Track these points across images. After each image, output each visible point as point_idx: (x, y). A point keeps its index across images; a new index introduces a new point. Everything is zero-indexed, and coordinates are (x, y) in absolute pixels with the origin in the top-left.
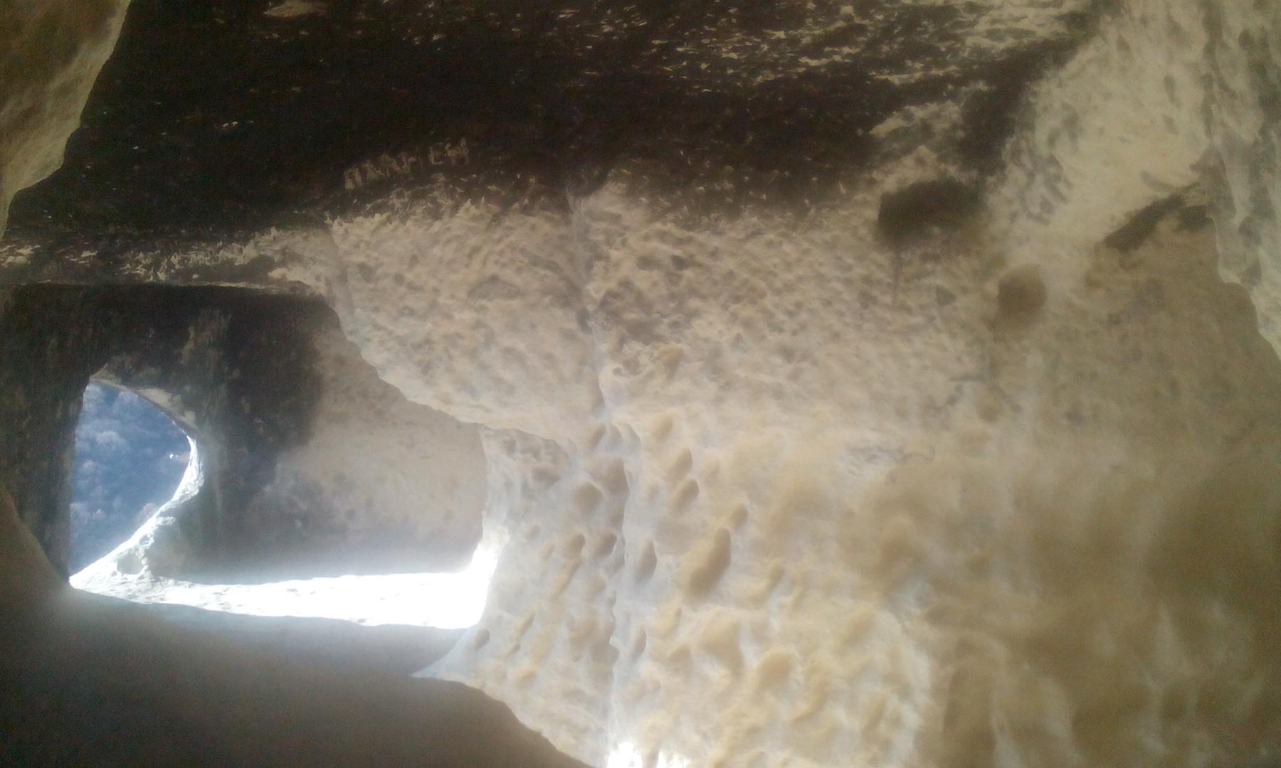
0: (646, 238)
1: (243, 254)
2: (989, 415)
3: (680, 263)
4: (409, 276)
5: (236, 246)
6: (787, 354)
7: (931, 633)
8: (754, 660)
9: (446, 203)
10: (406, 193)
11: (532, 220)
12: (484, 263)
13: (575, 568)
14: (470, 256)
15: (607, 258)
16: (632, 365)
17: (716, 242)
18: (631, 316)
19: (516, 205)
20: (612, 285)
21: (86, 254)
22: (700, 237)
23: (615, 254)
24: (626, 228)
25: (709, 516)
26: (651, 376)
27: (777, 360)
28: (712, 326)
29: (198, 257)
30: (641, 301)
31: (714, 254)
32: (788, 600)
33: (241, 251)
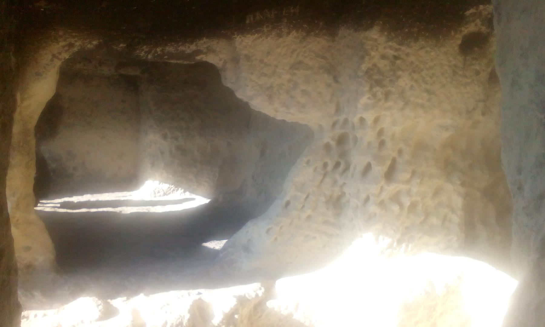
0: (385, 48)
1: (189, 48)
2: (483, 114)
3: (396, 58)
4: (266, 60)
5: (187, 45)
6: (428, 92)
7: (462, 190)
8: (407, 202)
9: (285, 30)
10: (270, 26)
11: (318, 39)
12: (298, 55)
13: (325, 175)
14: (292, 53)
15: (370, 55)
16: (374, 95)
17: (409, 50)
18: (375, 77)
19: (313, 33)
20: (370, 65)
21: (122, 45)
22: (403, 48)
23: (373, 53)
24: (379, 44)
25: (390, 151)
26: (380, 100)
27: (425, 94)
28: (404, 81)
29: (170, 49)
30: (379, 72)
31: (408, 55)
32: (419, 181)
33: (189, 47)
